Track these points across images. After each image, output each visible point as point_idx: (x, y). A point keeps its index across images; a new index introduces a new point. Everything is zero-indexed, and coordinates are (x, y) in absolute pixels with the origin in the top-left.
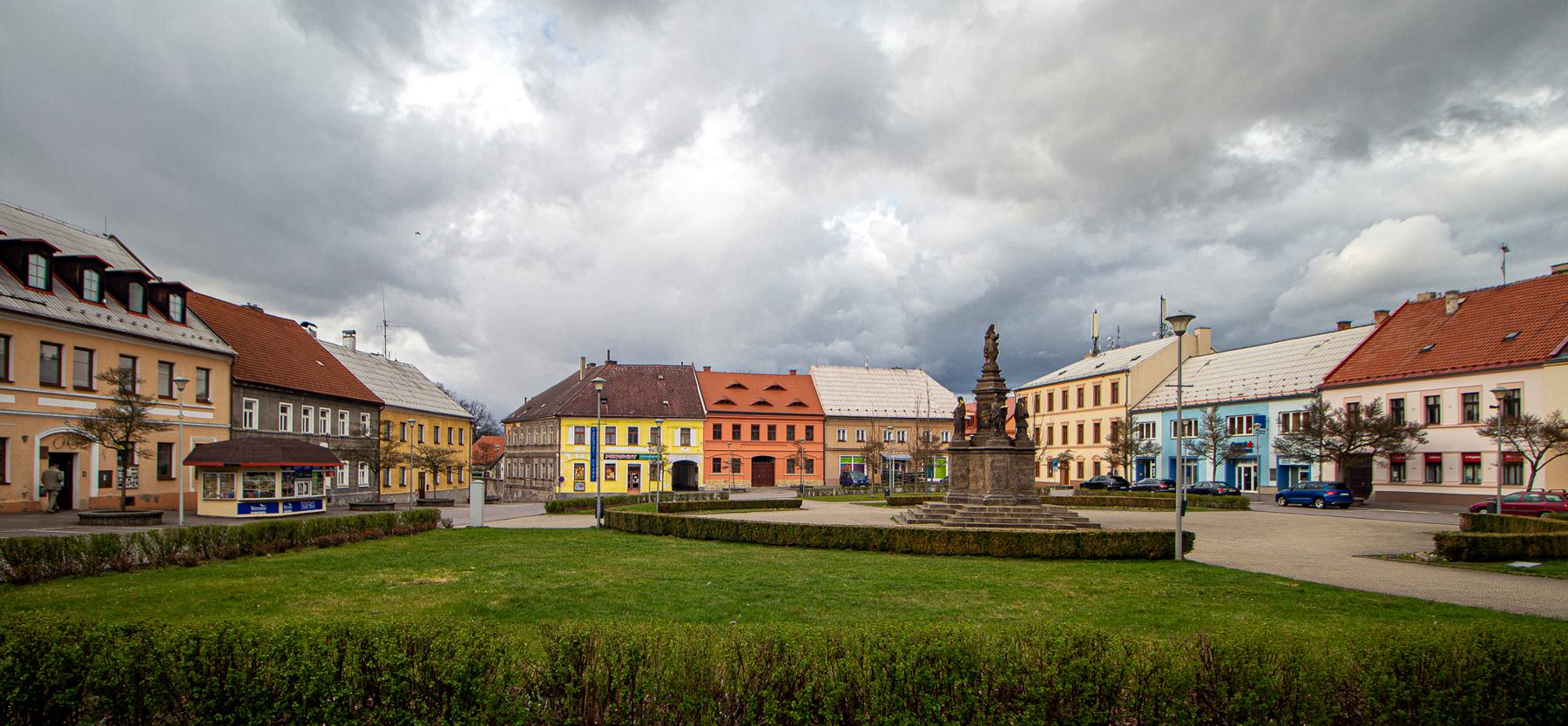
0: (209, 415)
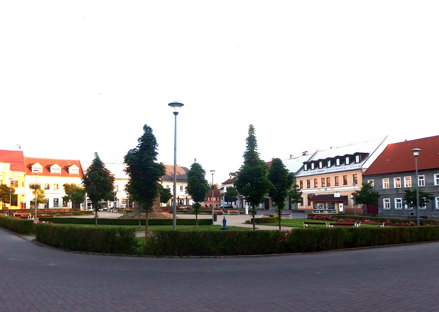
0: (317, 190)
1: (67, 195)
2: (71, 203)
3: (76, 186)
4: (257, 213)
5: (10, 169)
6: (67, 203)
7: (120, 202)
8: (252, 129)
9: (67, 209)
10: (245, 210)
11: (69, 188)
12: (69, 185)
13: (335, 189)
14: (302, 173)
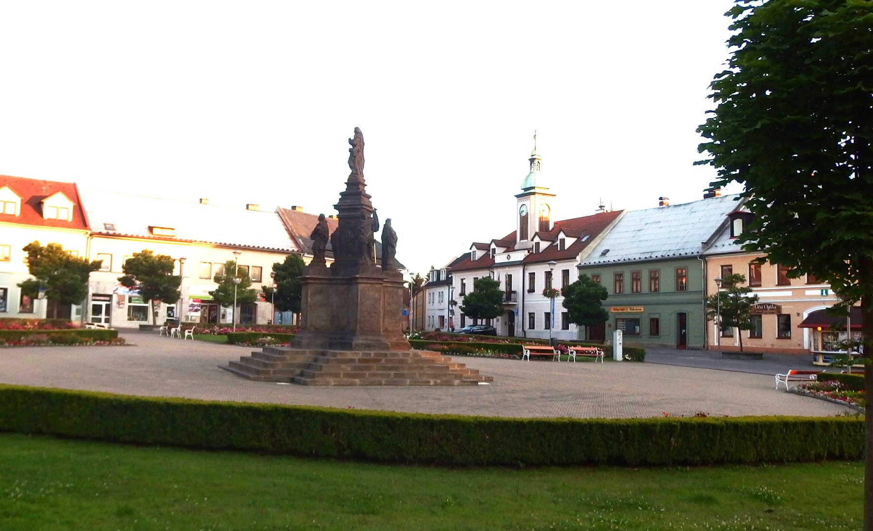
0: (790, 293)
1: (34, 278)
2: (45, 302)
3: (63, 253)
5: (74, 185)
6: (32, 303)
7: (186, 307)
8: (357, 145)
9: (32, 322)
11: (42, 255)
12: (41, 249)
13: (808, 293)
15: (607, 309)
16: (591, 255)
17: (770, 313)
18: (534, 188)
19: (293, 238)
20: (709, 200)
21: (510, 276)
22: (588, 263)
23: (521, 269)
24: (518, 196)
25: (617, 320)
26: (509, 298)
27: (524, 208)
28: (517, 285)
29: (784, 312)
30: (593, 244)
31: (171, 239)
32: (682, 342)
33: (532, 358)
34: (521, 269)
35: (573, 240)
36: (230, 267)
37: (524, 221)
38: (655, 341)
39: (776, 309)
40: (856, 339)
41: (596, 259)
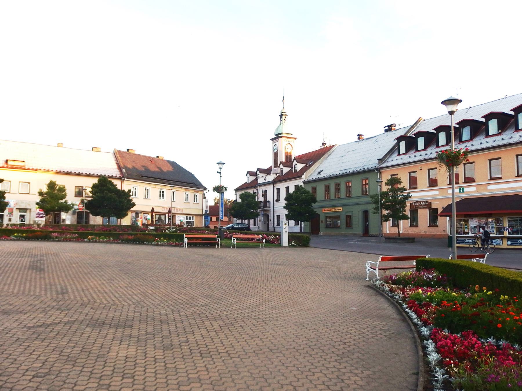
0: (437, 192)
4: (311, 244)
10: (278, 235)
13: (490, 187)
14: (395, 160)
15: (318, 211)
16: (311, 174)
17: (424, 208)
18: (281, 133)
19: (120, 168)
20: (388, 133)
21: (266, 191)
22: (309, 179)
23: (272, 186)
24: (272, 140)
25: (327, 217)
26: (266, 206)
27: (275, 147)
28: (270, 198)
29: (433, 206)
30: (314, 167)
31: (22, 168)
32: (366, 231)
33: (190, 245)
34: (272, 186)
35: (303, 165)
36: (52, 185)
37: (276, 155)
38: (350, 232)
39: (427, 205)
40: (483, 223)
41: (315, 176)
